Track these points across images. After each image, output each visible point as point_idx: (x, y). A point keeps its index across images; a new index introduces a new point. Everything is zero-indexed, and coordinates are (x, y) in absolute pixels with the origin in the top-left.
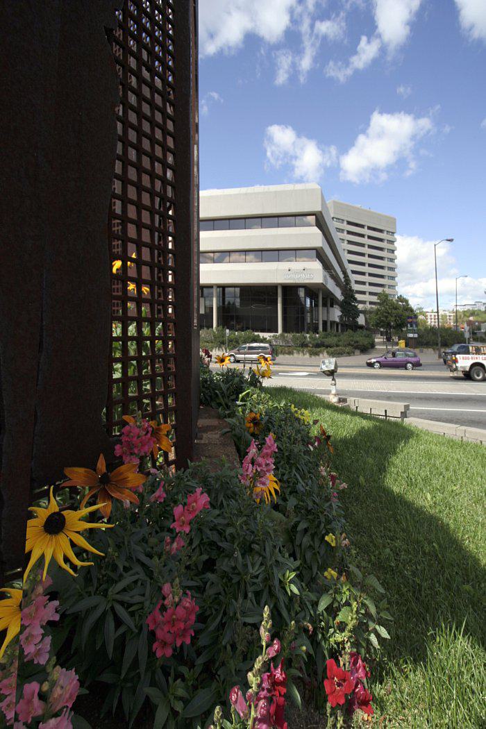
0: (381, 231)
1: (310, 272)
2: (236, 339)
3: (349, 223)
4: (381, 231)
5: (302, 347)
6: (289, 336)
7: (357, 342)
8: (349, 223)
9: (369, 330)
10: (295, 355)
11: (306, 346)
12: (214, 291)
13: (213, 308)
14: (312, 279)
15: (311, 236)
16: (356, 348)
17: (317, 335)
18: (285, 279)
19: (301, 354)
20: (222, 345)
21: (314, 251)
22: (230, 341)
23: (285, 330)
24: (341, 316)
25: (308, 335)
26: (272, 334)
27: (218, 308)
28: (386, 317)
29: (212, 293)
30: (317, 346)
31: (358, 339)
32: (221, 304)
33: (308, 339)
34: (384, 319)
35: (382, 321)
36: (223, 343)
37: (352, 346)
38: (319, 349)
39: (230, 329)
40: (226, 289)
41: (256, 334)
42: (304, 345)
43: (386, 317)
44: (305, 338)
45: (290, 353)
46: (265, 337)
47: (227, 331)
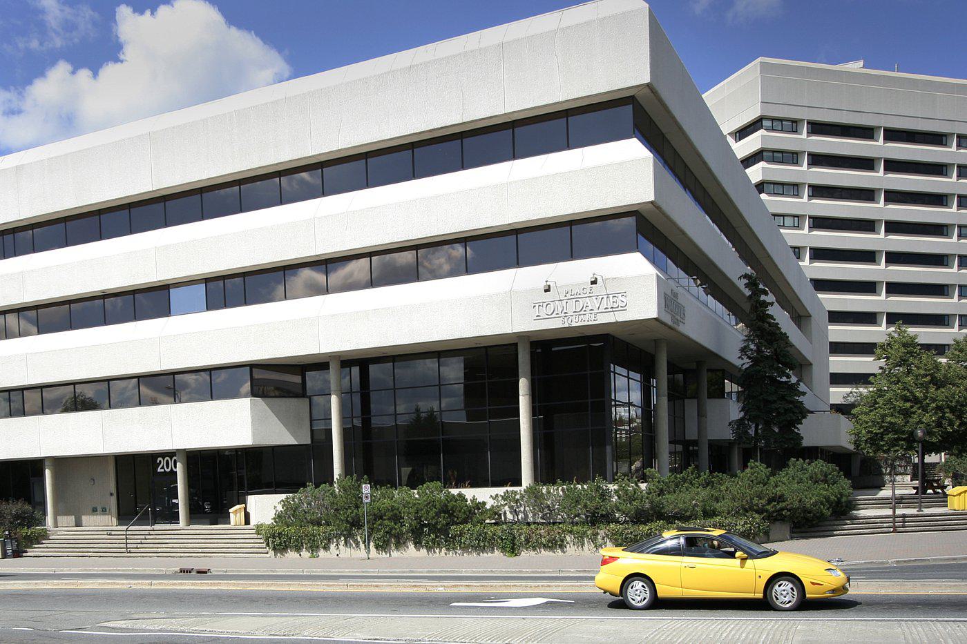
0: (937, 139)
1: (627, 288)
2: (393, 508)
3: (818, 128)
4: (937, 139)
5: (593, 524)
6: (557, 491)
7: (781, 498)
8: (818, 128)
9: (862, 470)
10: (571, 550)
11: (608, 519)
12: (333, 375)
13: (331, 430)
14: (623, 308)
15: (619, 172)
16: (775, 517)
17: (643, 486)
18: (538, 318)
19: (588, 547)
20: (354, 531)
21: (631, 221)
22: (378, 517)
23: (547, 472)
24: (740, 422)
25: (613, 487)
26: (501, 491)
27: (346, 434)
28: (906, 413)
29: (327, 382)
30: (640, 517)
31: (780, 490)
32: (357, 422)
33: (615, 499)
34: (899, 420)
35: (892, 428)
36: (356, 523)
37: (759, 512)
38: (644, 528)
39: (375, 483)
40: (373, 369)
41: (455, 491)
42: (598, 518)
43: (906, 413)
44: (604, 495)
45: (555, 544)
46: (480, 500)
47: (366, 489)
